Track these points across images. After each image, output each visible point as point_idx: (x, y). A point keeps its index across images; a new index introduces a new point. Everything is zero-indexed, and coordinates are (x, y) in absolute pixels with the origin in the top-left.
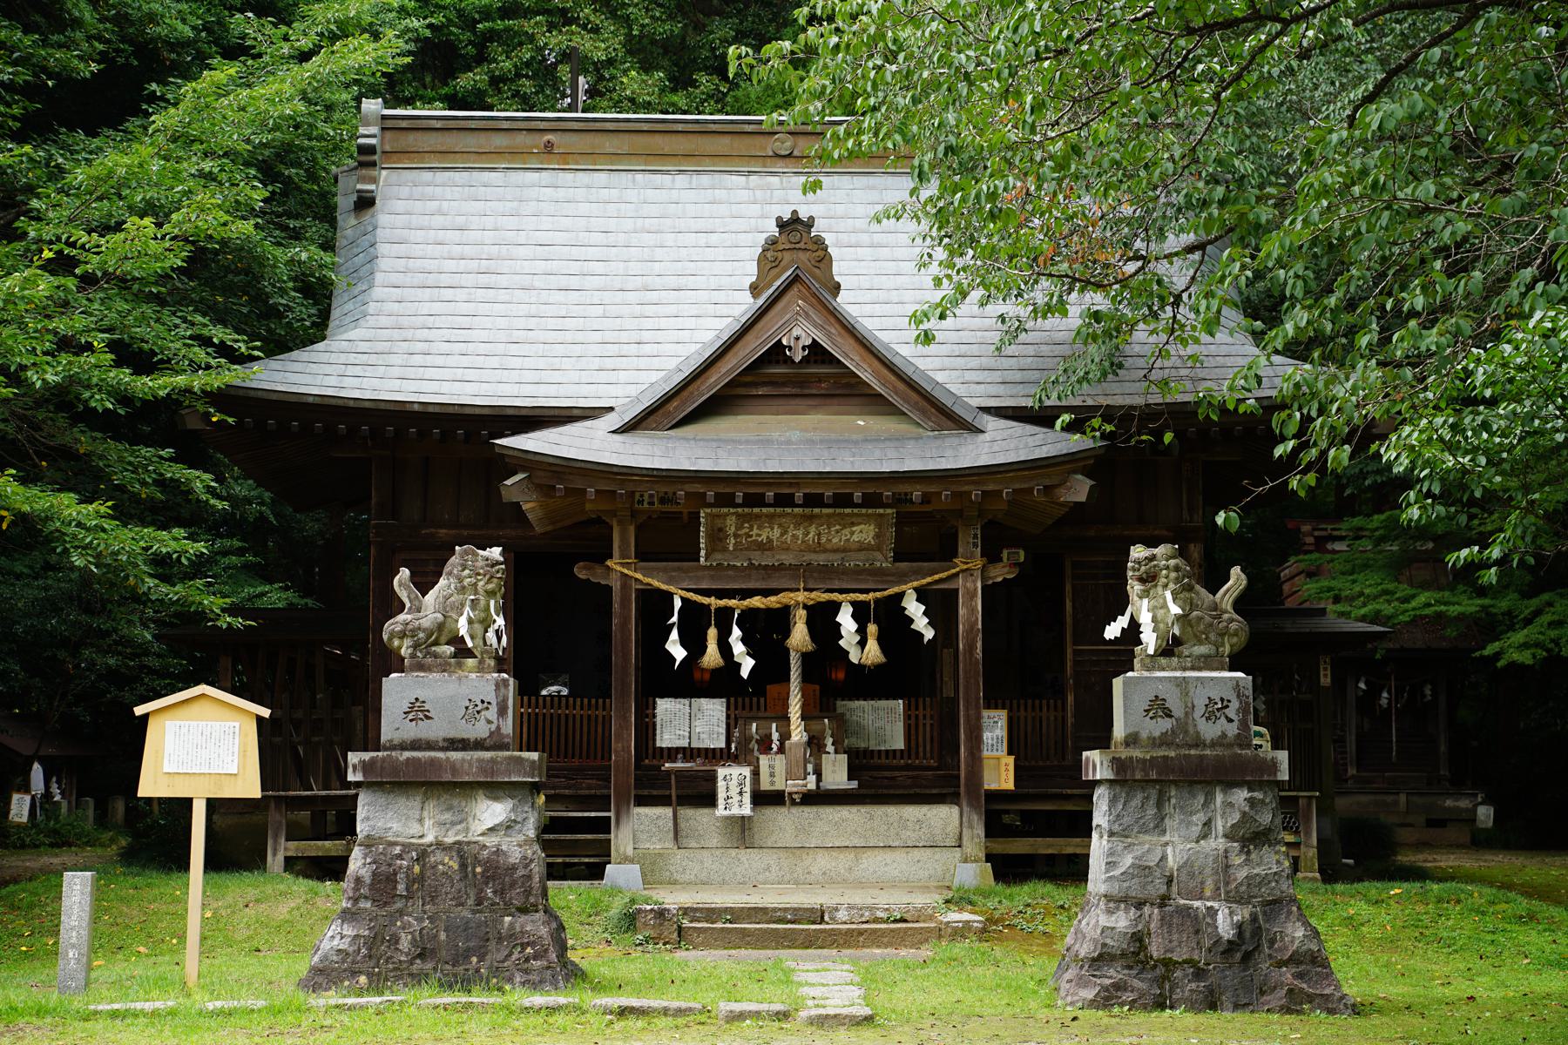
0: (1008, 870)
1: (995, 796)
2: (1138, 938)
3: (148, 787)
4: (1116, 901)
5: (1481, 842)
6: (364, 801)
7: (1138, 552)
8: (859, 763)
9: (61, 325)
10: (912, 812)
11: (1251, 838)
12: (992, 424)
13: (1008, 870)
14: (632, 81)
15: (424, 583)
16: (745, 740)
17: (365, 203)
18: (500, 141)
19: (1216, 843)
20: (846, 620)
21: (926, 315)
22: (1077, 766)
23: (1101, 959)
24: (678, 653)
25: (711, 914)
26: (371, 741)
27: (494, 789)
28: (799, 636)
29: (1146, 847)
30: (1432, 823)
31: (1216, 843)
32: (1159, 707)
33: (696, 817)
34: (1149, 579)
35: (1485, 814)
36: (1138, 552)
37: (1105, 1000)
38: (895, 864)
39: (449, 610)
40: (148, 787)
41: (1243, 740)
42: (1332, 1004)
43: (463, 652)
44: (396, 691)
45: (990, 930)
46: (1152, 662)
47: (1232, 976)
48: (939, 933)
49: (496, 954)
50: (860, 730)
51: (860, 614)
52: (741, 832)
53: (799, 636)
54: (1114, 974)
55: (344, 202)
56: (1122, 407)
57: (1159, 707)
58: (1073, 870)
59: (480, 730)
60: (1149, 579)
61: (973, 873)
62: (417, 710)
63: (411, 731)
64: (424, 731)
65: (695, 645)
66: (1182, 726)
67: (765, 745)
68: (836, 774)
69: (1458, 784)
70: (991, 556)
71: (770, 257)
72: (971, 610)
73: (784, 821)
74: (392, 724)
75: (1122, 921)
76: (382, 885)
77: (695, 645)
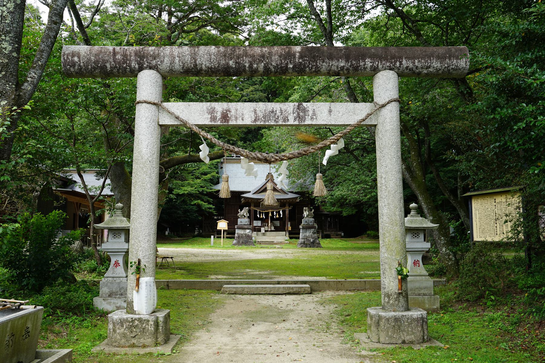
0: (291, 238)
1: (289, 231)
2: (304, 242)
3: (218, 228)
4: (302, 239)
5: (342, 237)
6: (236, 230)
7: (304, 208)
8: (275, 227)
9: (201, 185)
10: (281, 232)
11: (314, 233)
12: (289, 193)
13: (291, 238)
14: (240, 143)
15: (241, 211)
16: (263, 225)
17: (222, 168)
18: (235, 161)
19: (311, 234)
20: (275, 213)
21: (378, 324)
22: (299, 227)
23: (301, 244)
24: (259, 216)
25: (263, 242)
26: (237, 225)
27: (248, 229)
28: (270, 215)
29: (305, 234)
30: (336, 235)
31: (311, 234)
32: (306, 222)
33: (260, 233)
34: (305, 210)
35: (343, 234)
36: (304, 208)
37: (302, 247)
38: (279, 237)
39: (244, 213)
40: (218, 228)
41: (313, 225)
42: (321, 247)
43: (245, 217)
44: (239, 220)
45: (290, 243)
46: (306, 218)
47: (312, 245)
48: (285, 243)
49: (249, 243)
50: (275, 224)
51: (276, 212)
52: (264, 234)
53: (270, 215)
54: (302, 245)
55: (219, 167)
56: (278, 102)
57: (306, 222)
58: (298, 238)
59: (247, 224)
60: (305, 210)
61: (287, 238)
62: (241, 222)
63: (241, 224)
64: (242, 224)
65: (260, 216)
66: (308, 223)
67: (265, 226)
68: (273, 229)
69: (340, 231)
70: (289, 207)
71: (267, 176)
72: (287, 212)
73: (268, 233)
74: (239, 223)
75: (303, 240)
76: (239, 237)
77: (260, 216)
